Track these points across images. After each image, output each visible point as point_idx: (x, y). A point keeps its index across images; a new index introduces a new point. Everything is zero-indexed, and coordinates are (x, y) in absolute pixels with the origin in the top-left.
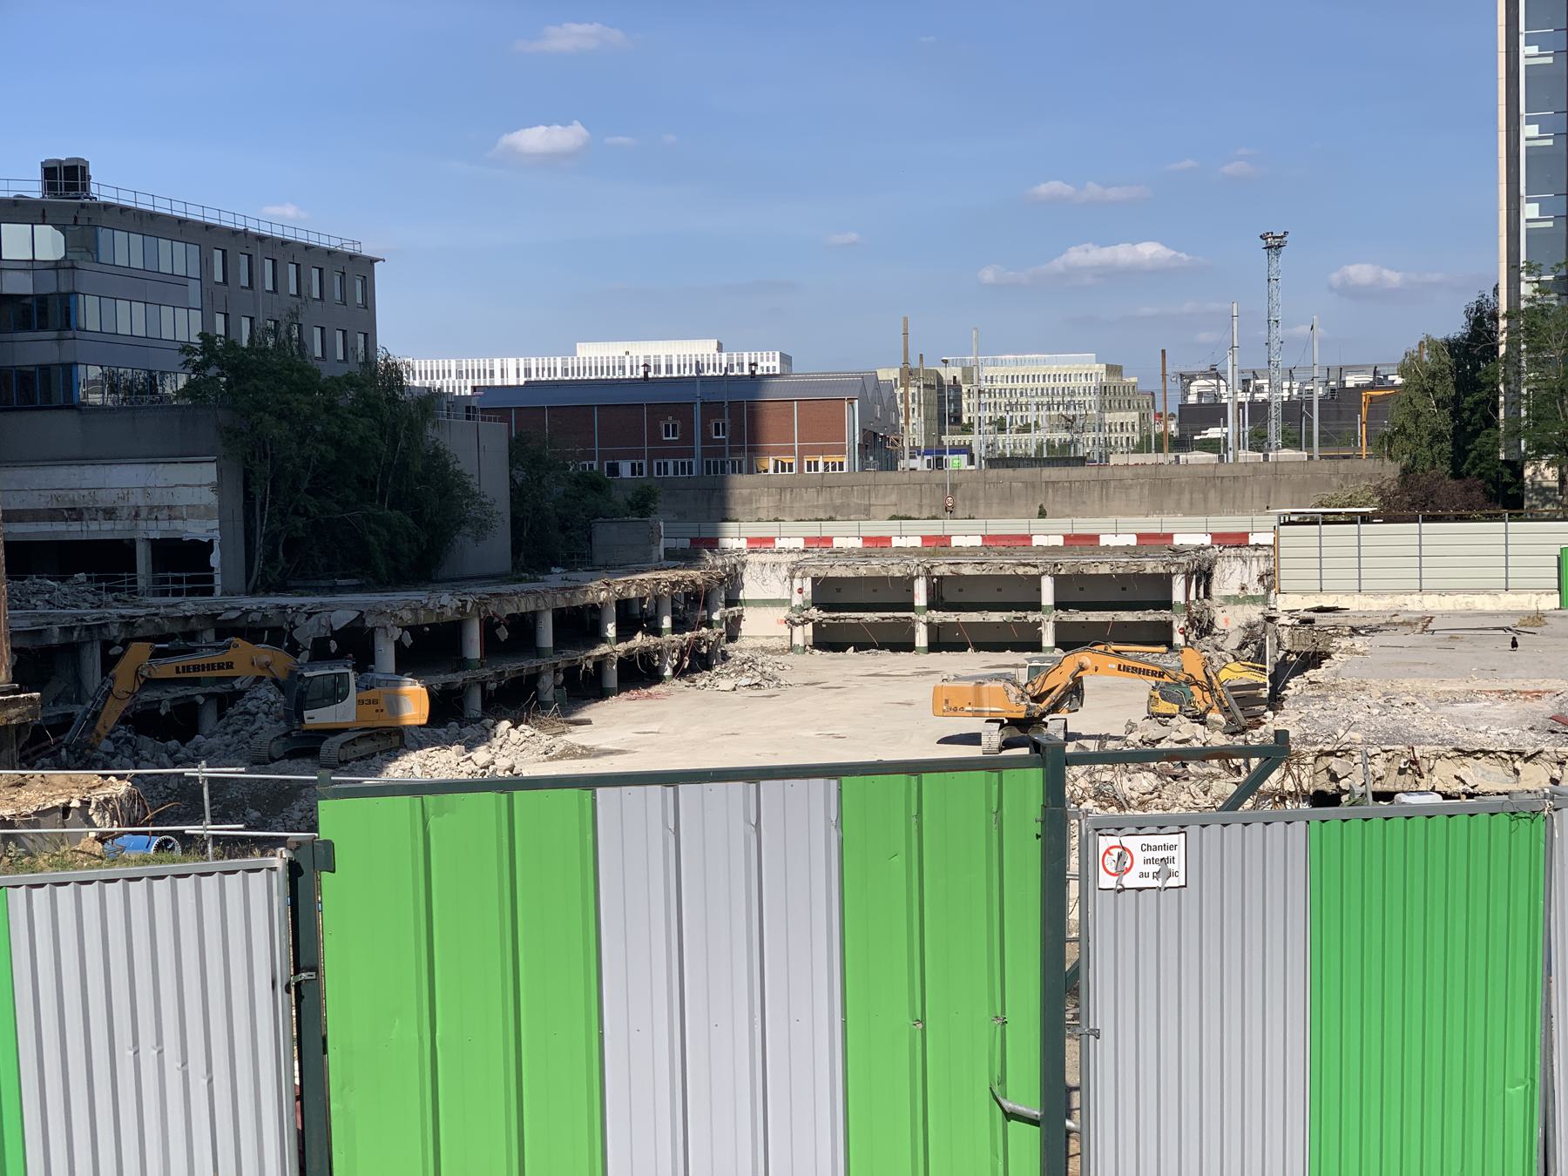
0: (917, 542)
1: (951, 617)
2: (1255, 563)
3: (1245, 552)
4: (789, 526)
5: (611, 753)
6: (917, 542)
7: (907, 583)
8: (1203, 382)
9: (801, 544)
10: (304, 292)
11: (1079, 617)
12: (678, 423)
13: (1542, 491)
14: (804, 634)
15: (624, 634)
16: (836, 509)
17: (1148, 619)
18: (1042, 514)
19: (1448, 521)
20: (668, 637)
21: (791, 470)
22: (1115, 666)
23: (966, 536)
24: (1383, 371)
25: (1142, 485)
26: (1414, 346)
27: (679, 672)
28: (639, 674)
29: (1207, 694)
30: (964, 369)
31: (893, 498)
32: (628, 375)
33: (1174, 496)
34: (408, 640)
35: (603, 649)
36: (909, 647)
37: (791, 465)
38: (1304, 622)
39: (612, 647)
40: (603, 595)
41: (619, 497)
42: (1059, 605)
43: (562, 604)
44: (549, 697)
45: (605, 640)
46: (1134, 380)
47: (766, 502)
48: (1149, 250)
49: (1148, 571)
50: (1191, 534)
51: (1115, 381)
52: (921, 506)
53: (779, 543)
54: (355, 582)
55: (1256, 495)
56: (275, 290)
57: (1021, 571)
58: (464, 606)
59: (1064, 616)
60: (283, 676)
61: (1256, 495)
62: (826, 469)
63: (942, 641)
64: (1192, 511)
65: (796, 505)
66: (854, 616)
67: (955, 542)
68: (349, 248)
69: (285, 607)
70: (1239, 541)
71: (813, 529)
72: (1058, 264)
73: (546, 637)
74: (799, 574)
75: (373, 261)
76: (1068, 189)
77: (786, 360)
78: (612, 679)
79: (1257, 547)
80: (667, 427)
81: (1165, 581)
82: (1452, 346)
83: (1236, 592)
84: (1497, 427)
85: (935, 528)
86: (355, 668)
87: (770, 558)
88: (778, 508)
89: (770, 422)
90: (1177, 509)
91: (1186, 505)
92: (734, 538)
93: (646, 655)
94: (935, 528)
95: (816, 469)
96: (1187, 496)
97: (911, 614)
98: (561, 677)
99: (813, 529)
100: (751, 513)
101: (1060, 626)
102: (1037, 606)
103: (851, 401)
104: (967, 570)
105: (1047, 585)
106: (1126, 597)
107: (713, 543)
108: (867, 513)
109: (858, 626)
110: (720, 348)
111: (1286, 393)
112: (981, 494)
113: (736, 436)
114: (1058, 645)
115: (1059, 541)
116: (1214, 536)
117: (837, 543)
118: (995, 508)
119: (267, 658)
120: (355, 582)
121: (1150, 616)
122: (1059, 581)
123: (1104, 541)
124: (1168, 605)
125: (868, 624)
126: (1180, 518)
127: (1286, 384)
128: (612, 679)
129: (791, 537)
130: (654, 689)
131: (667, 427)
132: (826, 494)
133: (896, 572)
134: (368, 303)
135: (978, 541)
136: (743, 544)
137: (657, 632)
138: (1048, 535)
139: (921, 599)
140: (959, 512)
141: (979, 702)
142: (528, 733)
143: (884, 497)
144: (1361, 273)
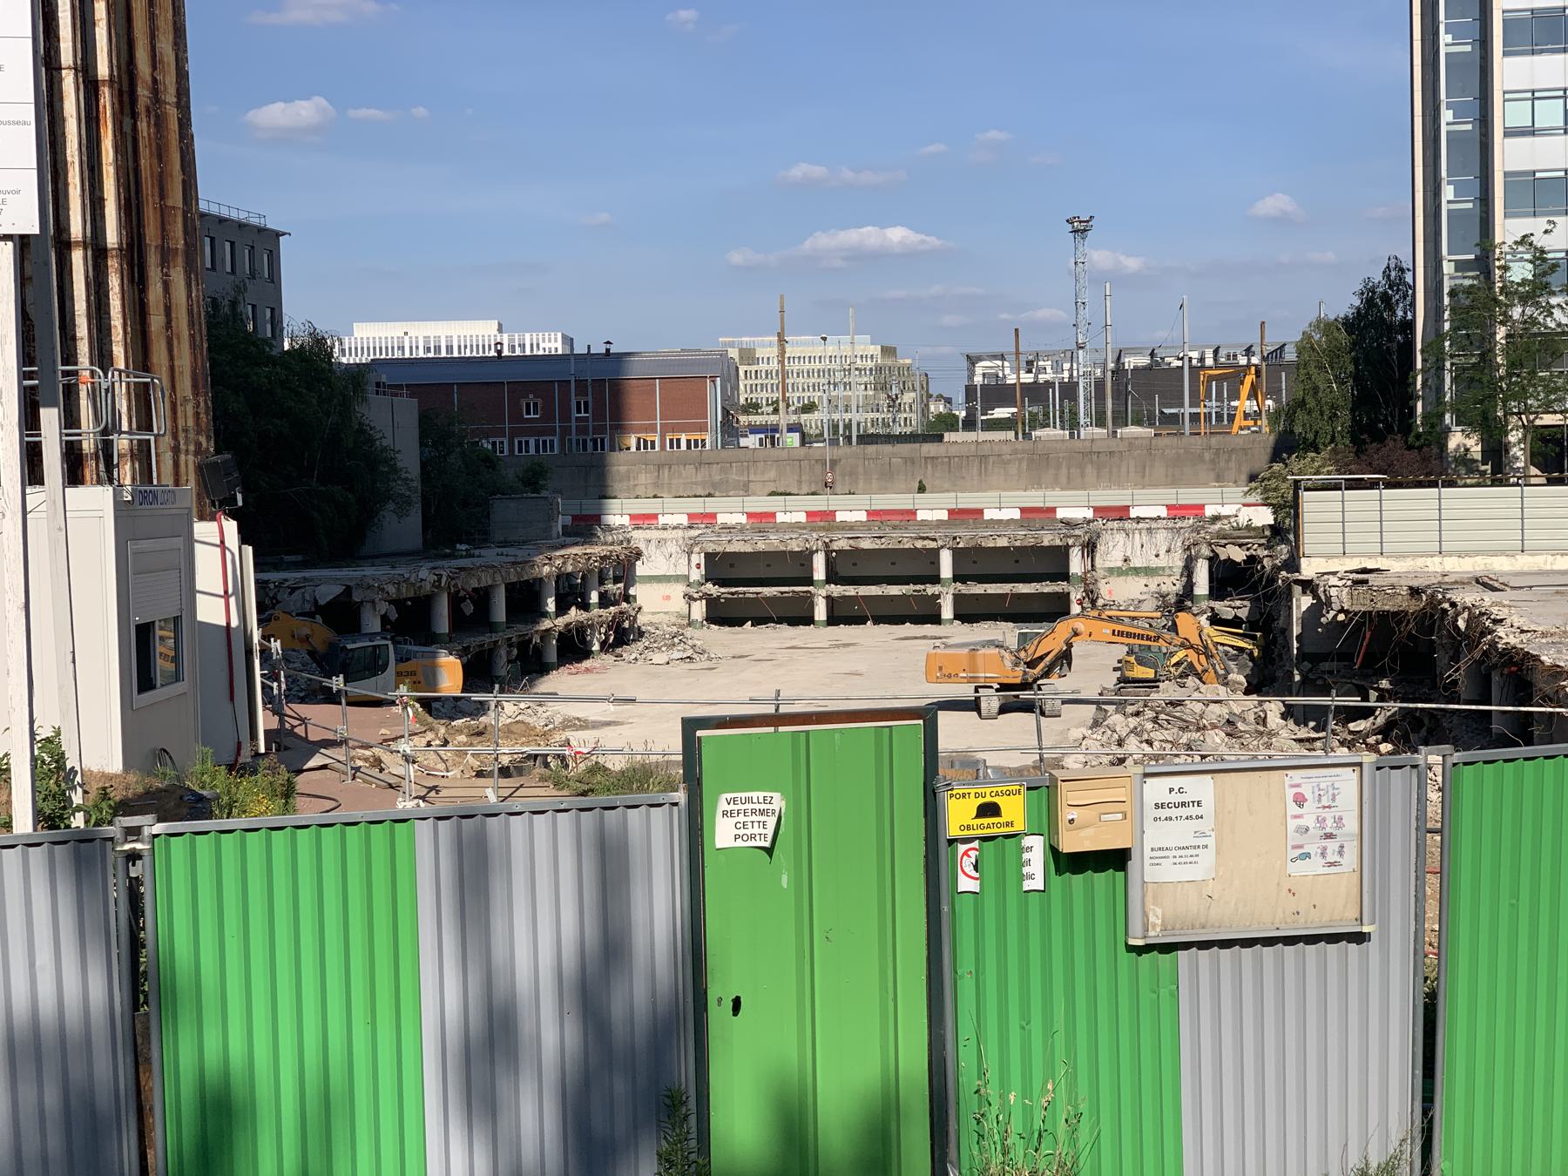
0: (802, 518)
1: (850, 591)
2: (1137, 536)
3: (1128, 525)
4: (670, 503)
5: (608, 724)
6: (802, 518)
7: (805, 557)
8: (988, 363)
9: (684, 520)
10: (218, 267)
11: (978, 589)
12: (539, 401)
14: (699, 610)
15: (562, 609)
16: (714, 485)
17: (1046, 590)
18: (922, 489)
19: (1408, 486)
20: (596, 611)
21: (653, 447)
22: (1109, 632)
23: (851, 511)
24: (1160, 353)
25: (1020, 460)
26: (1304, 327)
27: (605, 647)
28: (574, 648)
29: (1202, 658)
30: (741, 350)
31: (772, 474)
32: (407, 355)
33: (1052, 471)
34: (394, 616)
35: (546, 624)
36: (808, 620)
37: (653, 442)
38: (1356, 582)
39: (554, 622)
40: (546, 569)
41: (510, 474)
42: (958, 578)
43: (514, 579)
44: (503, 672)
45: (545, 615)
46: (908, 361)
48: (896, 234)
49: (1046, 543)
50: (1074, 507)
51: (889, 362)
52: (800, 482)
53: (662, 520)
54: (300, 558)
55: (1132, 469)
56: (213, 268)
57: (919, 544)
58: (439, 581)
59: (964, 589)
61: (1132, 469)
62: (689, 447)
64: (1069, 486)
65: (674, 481)
66: (748, 590)
67: (840, 517)
68: (254, 221)
69: (267, 582)
70: (1121, 514)
71: (697, 506)
72: (808, 244)
73: (500, 613)
74: (696, 549)
75: (278, 234)
76: (818, 171)
77: (568, 341)
78: (552, 656)
79: (1139, 520)
80: (528, 405)
81: (1062, 553)
82: (1350, 325)
83: (1120, 564)
85: (819, 503)
86: (392, 639)
88: (656, 485)
89: (634, 400)
90: (1055, 483)
91: (1064, 480)
92: (617, 514)
93: (581, 629)
94: (819, 503)
95: (679, 446)
96: (1064, 471)
97: (811, 588)
98: (515, 652)
99: (697, 506)
100: (628, 491)
101: (958, 598)
102: (936, 579)
103: (713, 379)
104: (866, 544)
105: (946, 559)
106: (1011, 569)
108: (746, 489)
109: (757, 601)
110: (500, 330)
111: (1066, 374)
112: (861, 470)
113: (599, 415)
114: (957, 617)
115: (944, 516)
116: (1096, 509)
117: (721, 519)
118: (875, 484)
119: (306, 631)
120: (300, 558)
121: (1047, 588)
122: (958, 554)
123: (988, 515)
124: (1065, 576)
125: (767, 599)
126: (1057, 492)
127: (1067, 366)
128: (552, 656)
129: (674, 513)
130: (587, 664)
131: (528, 405)
132: (704, 471)
133: (795, 546)
135: (863, 516)
136: (626, 520)
138: (932, 510)
139: (819, 573)
140: (838, 488)
141: (974, 669)
142: (522, 705)
143: (763, 473)
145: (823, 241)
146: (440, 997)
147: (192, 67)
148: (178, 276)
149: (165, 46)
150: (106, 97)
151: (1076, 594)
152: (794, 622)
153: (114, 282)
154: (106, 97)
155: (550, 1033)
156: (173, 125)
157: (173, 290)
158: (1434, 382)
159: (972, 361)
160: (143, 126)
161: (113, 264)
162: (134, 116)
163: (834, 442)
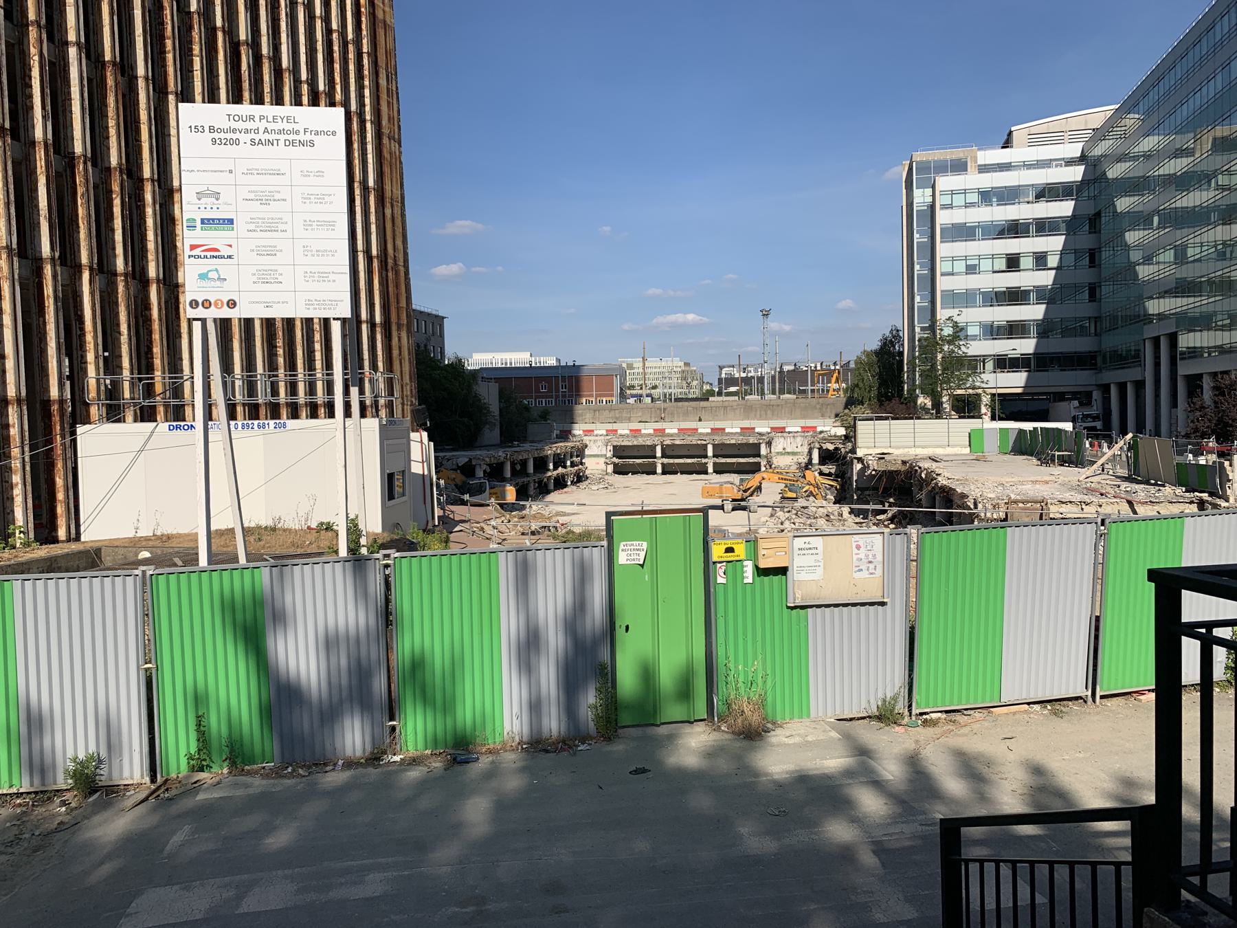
1: (671, 461)
7: (653, 447)
13: (924, 408)
14: (610, 468)
15: (555, 468)
23: (671, 429)
28: (560, 483)
35: (549, 474)
36: (654, 473)
39: (552, 473)
41: (535, 414)
47: (588, 416)
50: (763, 427)
60: (460, 484)
63: (719, 470)
64: (761, 418)
66: (631, 460)
71: (610, 427)
73: (531, 469)
78: (552, 486)
81: (758, 446)
84: (166, 406)
85: (659, 426)
87: (592, 438)
89: (584, 384)
90: (755, 418)
92: (578, 430)
93: (563, 476)
94: (659, 426)
99: (610, 427)
101: (715, 464)
102: (706, 457)
104: (677, 442)
107: (569, 432)
108: (629, 420)
113: (570, 390)
121: (751, 460)
122: (715, 446)
124: (759, 456)
128: (552, 486)
129: (600, 430)
134: (442, 336)
137: (565, 467)
138: (704, 428)
139: (659, 454)
144: (626, 327)
145: (660, 320)
146: (509, 624)
147: (409, 251)
148: (404, 334)
149: (399, 243)
150: (376, 263)
151: (763, 463)
152: (648, 473)
153: (379, 337)
154: (376, 263)
155: (555, 641)
156: (402, 274)
157: (402, 340)
158: (911, 377)
159: (721, 368)
160: (390, 274)
161: (378, 329)
162: (387, 270)
163: (665, 401)
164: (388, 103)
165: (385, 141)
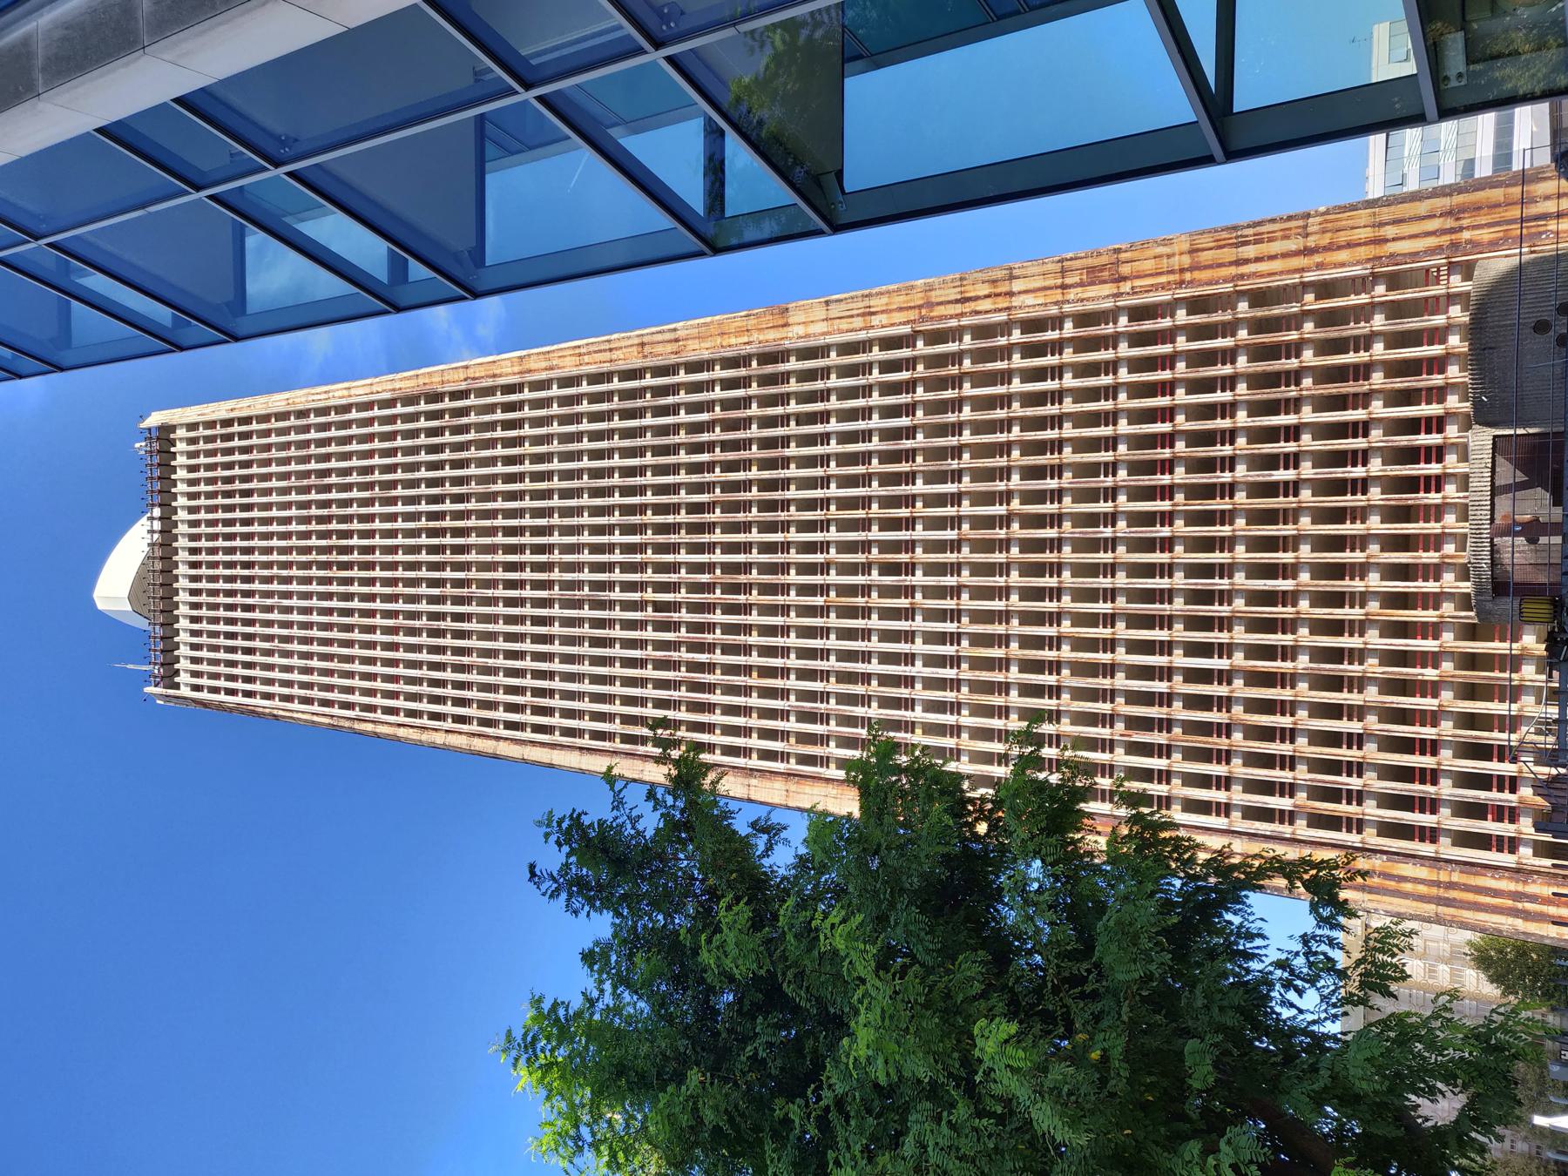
164: (1271, 240)
165: (1311, 242)
